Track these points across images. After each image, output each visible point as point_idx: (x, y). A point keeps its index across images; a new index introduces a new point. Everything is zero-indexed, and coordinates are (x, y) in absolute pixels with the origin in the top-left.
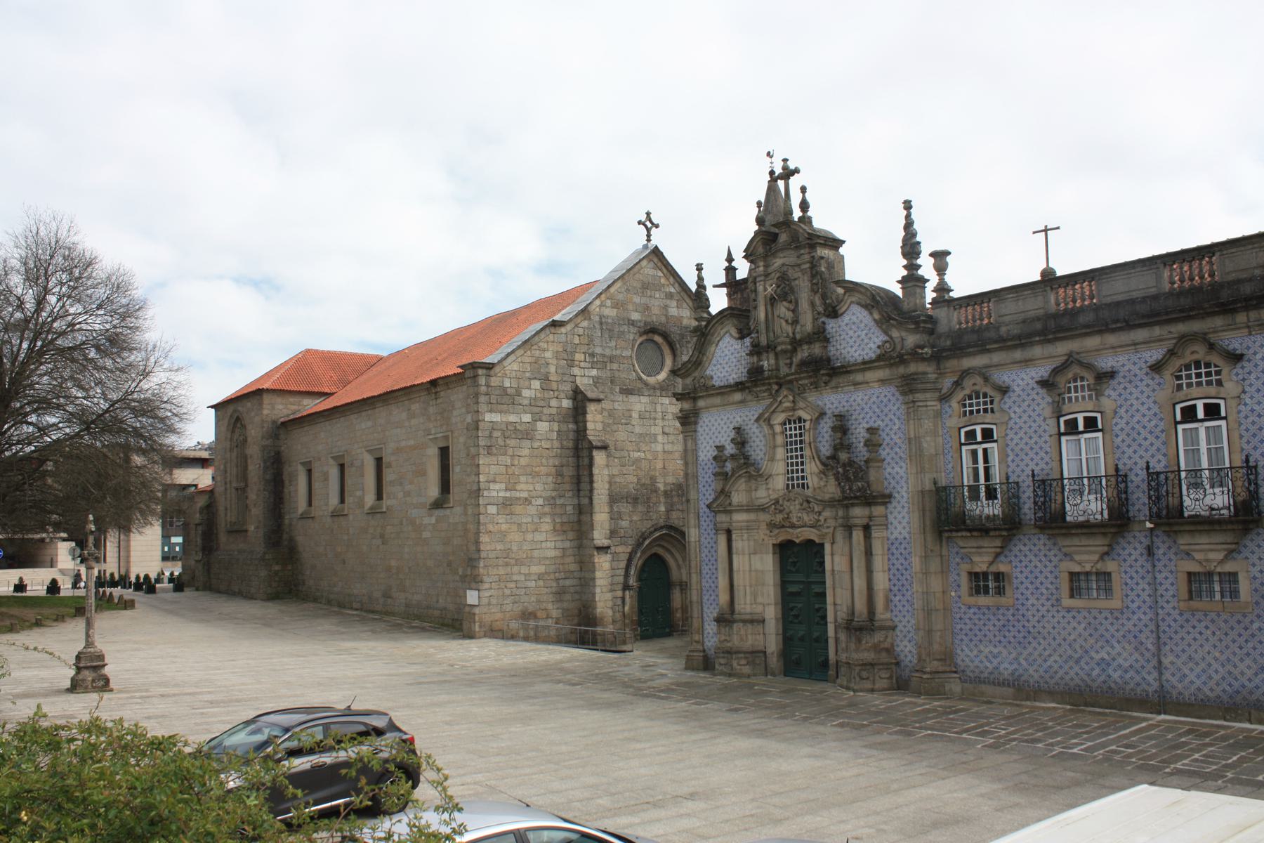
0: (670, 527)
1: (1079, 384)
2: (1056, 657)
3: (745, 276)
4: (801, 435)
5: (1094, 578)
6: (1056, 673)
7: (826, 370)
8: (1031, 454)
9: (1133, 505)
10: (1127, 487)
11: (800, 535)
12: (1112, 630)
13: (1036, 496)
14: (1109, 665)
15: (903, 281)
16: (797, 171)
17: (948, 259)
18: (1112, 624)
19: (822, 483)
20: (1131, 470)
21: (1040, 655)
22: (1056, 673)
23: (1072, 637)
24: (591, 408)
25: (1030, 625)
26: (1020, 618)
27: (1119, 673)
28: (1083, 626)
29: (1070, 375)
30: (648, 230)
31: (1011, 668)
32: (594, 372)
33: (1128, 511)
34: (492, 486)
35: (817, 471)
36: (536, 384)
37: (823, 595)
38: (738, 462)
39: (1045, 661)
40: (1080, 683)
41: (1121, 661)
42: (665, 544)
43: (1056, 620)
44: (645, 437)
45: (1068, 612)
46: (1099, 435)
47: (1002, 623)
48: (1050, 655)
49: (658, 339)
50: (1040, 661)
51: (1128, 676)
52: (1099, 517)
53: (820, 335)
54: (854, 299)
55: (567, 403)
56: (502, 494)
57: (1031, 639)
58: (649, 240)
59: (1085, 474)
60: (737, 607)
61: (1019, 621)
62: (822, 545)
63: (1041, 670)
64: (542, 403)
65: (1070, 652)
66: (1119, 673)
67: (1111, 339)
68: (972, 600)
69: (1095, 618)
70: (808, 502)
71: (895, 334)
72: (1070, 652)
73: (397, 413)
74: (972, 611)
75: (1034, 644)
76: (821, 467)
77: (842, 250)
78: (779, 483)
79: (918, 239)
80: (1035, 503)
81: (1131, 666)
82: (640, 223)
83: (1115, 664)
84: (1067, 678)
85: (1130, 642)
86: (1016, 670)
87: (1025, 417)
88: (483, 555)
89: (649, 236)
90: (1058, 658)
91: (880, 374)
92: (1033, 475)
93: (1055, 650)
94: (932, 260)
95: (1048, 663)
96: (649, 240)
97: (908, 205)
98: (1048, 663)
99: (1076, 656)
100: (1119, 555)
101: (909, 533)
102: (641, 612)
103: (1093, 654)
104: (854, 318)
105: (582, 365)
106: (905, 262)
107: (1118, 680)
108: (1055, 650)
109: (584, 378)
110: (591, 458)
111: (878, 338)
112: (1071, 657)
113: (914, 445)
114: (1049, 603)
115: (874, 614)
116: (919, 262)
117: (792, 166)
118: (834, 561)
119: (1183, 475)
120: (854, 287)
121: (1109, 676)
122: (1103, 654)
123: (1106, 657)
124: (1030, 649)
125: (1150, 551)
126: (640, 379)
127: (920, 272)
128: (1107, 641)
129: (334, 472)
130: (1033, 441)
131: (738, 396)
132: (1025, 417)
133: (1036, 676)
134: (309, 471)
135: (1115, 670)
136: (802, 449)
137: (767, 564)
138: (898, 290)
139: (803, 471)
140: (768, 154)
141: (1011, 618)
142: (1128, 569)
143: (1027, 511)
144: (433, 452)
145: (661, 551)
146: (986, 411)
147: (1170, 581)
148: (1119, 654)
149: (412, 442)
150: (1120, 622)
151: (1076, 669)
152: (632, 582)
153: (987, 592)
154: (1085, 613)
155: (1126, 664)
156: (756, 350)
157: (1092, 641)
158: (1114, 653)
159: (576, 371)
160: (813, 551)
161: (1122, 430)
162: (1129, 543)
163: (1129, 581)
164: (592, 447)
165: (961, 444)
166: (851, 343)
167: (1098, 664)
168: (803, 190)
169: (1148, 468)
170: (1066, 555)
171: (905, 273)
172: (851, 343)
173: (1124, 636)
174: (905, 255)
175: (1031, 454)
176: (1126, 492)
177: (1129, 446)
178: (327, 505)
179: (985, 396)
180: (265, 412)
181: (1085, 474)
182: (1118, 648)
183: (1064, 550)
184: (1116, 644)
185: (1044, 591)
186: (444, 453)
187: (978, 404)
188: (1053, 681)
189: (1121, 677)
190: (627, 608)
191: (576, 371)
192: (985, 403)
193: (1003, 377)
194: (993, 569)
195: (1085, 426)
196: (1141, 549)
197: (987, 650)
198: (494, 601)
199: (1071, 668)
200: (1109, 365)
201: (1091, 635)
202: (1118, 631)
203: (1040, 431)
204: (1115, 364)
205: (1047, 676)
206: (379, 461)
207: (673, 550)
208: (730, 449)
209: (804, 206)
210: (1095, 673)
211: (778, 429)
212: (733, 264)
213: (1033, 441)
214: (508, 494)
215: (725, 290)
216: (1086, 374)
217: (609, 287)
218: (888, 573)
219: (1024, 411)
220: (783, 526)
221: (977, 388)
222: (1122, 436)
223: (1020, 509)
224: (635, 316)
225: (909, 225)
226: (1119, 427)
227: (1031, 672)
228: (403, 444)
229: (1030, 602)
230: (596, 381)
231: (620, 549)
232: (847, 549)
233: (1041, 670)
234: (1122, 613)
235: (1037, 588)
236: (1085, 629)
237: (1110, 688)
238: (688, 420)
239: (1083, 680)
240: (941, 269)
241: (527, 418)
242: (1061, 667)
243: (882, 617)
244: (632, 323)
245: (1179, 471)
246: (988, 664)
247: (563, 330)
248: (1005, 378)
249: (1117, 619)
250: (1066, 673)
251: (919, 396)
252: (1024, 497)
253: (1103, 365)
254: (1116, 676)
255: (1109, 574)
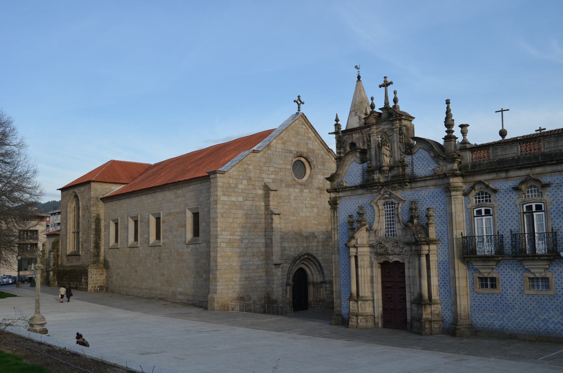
0: (308, 254)
1: (533, 189)
3: (344, 129)
4: (393, 211)
5: (540, 280)
6: (522, 325)
7: (402, 179)
8: (510, 222)
9: (559, 246)
10: (556, 238)
11: (393, 259)
12: (549, 305)
13: (512, 242)
14: (548, 321)
15: (446, 138)
16: (391, 83)
17: (468, 128)
18: (549, 302)
19: (404, 234)
20: (558, 230)
21: (514, 317)
22: (522, 325)
23: (530, 308)
24: (272, 193)
25: (509, 302)
26: (504, 299)
27: (553, 325)
28: (535, 303)
29: (529, 185)
30: (299, 105)
31: (499, 323)
32: (273, 176)
33: (557, 249)
34: (224, 233)
35: (401, 228)
36: (245, 182)
38: (355, 224)
39: (517, 319)
40: (534, 330)
41: (554, 319)
42: (305, 262)
43: (522, 300)
44: (305, 211)
45: (528, 296)
46: (543, 213)
47: (494, 301)
48: (519, 317)
49: (302, 159)
50: (514, 320)
51: (557, 327)
52: (543, 251)
54: (420, 146)
55: (260, 192)
56: (228, 237)
57: (509, 309)
58: (299, 110)
59: (485, 234)
60: (361, 294)
61: (503, 301)
62: (404, 264)
63: (515, 324)
64: (247, 192)
65: (529, 315)
66: (553, 325)
67: (549, 169)
68: (481, 291)
69: (541, 299)
70: (397, 243)
72: (529, 315)
73: (168, 195)
74: (480, 295)
75: (511, 311)
76: (403, 226)
77: (413, 122)
79: (453, 118)
80: (512, 244)
81: (559, 322)
82: (295, 101)
83: (551, 321)
85: (558, 311)
86: (502, 324)
87: (506, 204)
88: (219, 268)
89: (299, 108)
90: (522, 318)
91: (433, 182)
92: (511, 232)
93: (521, 315)
94: (460, 129)
95: (518, 321)
96: (299, 110)
97: (448, 102)
98: (518, 321)
99: (532, 317)
100: (553, 269)
101: (449, 258)
102: (294, 297)
103: (540, 316)
104: (421, 155)
105: (268, 172)
106: (446, 129)
107: (553, 329)
109: (268, 179)
110: (272, 219)
112: (529, 318)
113: (460, 215)
114: (518, 292)
115: (431, 296)
116: (453, 129)
117: (389, 80)
119: (526, 235)
120: (420, 140)
121: (548, 327)
123: (547, 317)
124: (509, 314)
126: (295, 180)
127: (454, 134)
128: (547, 310)
129: (131, 225)
130: (510, 215)
131: (360, 191)
132: (506, 204)
133: (512, 327)
134: (117, 224)
135: (551, 324)
136: (393, 217)
138: (442, 142)
139: (393, 228)
140: (356, 67)
141: (499, 299)
142: (557, 276)
143: (507, 248)
144: (189, 215)
145: (303, 266)
146: (486, 201)
147: (558, 290)
148: (553, 316)
149: (177, 210)
150: (553, 301)
151: (532, 323)
152: (291, 281)
153: (487, 287)
154: (536, 297)
155: (556, 321)
158: (551, 315)
159: (264, 176)
160: (400, 266)
161: (554, 211)
162: (558, 264)
163: (557, 282)
164: (273, 213)
165: (474, 217)
166: (419, 167)
167: (542, 321)
168: (395, 93)
169: (462, 235)
170: (526, 269)
171: (446, 134)
172: (419, 167)
173: (555, 308)
174: (446, 126)
175: (510, 222)
176: (556, 240)
177: (557, 219)
178: (127, 241)
179: (486, 194)
180: (92, 193)
181: (485, 234)
182: (552, 313)
183: (526, 267)
184: (551, 312)
185: (516, 286)
186: (196, 216)
187: (483, 198)
188: (520, 329)
189: (554, 327)
190: (288, 296)
191: (264, 176)
192: (486, 197)
194: (491, 276)
195: (536, 209)
197: (487, 314)
198: (224, 291)
199: (529, 323)
200: (548, 180)
201: (539, 307)
202: (552, 305)
203: (514, 211)
204: (550, 180)
206: (158, 219)
207: (310, 267)
208: (356, 217)
209: (395, 100)
210: (541, 325)
211: (381, 207)
212: (339, 122)
213: (510, 215)
214: (231, 237)
215: (334, 135)
216: (537, 185)
217: (280, 133)
218: (436, 277)
219: (506, 202)
220: (384, 255)
221: (482, 190)
222: (554, 214)
223: (503, 248)
224: (292, 148)
225: (448, 112)
226: (553, 210)
227: (509, 325)
228: (172, 211)
229: (509, 292)
230: (274, 181)
231: (285, 265)
233: (515, 324)
234: (554, 297)
235: (512, 285)
236: (536, 304)
237: (548, 332)
238: (334, 204)
240: (464, 133)
241: (241, 199)
242: (524, 322)
243: (435, 298)
244: (291, 152)
245: (525, 234)
246: (488, 321)
247: (258, 155)
248: (496, 185)
249: (552, 299)
250: (527, 325)
251: (453, 193)
252: (505, 242)
253: (545, 181)
254: (551, 326)
255: (548, 278)
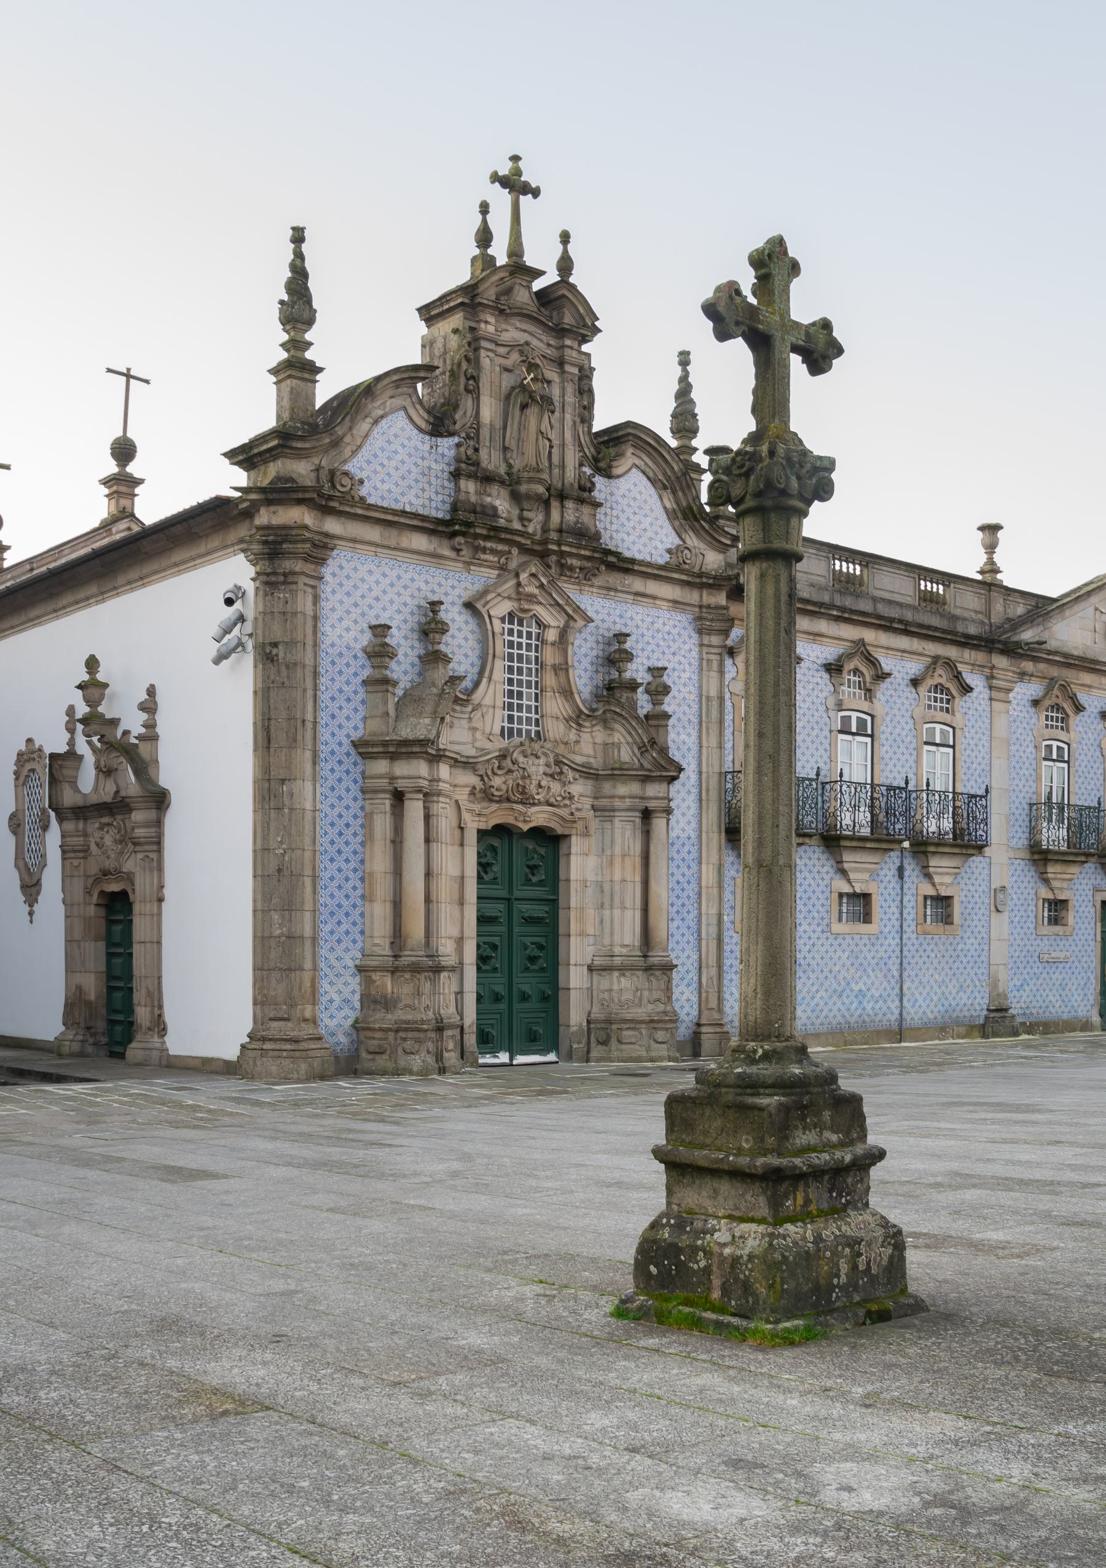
2: (822, 993)
23: (837, 968)
37: (482, 920)
39: (813, 998)
51: (877, 1007)
53: (584, 494)
54: (638, 462)
71: (692, 541)
78: (497, 721)
84: (831, 1015)
108: (822, 985)
111: (673, 540)
114: (820, 929)
118: (581, 865)
122: (861, 986)
125: (901, 870)
131: (420, 542)
137: (458, 862)
154: (848, 939)
156: (465, 468)
157: (852, 971)
193: (887, 663)
196: (894, 871)
205: (813, 1016)
232: (637, 847)
239: (843, 1016)
